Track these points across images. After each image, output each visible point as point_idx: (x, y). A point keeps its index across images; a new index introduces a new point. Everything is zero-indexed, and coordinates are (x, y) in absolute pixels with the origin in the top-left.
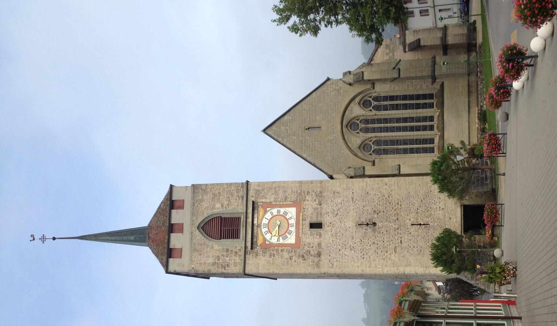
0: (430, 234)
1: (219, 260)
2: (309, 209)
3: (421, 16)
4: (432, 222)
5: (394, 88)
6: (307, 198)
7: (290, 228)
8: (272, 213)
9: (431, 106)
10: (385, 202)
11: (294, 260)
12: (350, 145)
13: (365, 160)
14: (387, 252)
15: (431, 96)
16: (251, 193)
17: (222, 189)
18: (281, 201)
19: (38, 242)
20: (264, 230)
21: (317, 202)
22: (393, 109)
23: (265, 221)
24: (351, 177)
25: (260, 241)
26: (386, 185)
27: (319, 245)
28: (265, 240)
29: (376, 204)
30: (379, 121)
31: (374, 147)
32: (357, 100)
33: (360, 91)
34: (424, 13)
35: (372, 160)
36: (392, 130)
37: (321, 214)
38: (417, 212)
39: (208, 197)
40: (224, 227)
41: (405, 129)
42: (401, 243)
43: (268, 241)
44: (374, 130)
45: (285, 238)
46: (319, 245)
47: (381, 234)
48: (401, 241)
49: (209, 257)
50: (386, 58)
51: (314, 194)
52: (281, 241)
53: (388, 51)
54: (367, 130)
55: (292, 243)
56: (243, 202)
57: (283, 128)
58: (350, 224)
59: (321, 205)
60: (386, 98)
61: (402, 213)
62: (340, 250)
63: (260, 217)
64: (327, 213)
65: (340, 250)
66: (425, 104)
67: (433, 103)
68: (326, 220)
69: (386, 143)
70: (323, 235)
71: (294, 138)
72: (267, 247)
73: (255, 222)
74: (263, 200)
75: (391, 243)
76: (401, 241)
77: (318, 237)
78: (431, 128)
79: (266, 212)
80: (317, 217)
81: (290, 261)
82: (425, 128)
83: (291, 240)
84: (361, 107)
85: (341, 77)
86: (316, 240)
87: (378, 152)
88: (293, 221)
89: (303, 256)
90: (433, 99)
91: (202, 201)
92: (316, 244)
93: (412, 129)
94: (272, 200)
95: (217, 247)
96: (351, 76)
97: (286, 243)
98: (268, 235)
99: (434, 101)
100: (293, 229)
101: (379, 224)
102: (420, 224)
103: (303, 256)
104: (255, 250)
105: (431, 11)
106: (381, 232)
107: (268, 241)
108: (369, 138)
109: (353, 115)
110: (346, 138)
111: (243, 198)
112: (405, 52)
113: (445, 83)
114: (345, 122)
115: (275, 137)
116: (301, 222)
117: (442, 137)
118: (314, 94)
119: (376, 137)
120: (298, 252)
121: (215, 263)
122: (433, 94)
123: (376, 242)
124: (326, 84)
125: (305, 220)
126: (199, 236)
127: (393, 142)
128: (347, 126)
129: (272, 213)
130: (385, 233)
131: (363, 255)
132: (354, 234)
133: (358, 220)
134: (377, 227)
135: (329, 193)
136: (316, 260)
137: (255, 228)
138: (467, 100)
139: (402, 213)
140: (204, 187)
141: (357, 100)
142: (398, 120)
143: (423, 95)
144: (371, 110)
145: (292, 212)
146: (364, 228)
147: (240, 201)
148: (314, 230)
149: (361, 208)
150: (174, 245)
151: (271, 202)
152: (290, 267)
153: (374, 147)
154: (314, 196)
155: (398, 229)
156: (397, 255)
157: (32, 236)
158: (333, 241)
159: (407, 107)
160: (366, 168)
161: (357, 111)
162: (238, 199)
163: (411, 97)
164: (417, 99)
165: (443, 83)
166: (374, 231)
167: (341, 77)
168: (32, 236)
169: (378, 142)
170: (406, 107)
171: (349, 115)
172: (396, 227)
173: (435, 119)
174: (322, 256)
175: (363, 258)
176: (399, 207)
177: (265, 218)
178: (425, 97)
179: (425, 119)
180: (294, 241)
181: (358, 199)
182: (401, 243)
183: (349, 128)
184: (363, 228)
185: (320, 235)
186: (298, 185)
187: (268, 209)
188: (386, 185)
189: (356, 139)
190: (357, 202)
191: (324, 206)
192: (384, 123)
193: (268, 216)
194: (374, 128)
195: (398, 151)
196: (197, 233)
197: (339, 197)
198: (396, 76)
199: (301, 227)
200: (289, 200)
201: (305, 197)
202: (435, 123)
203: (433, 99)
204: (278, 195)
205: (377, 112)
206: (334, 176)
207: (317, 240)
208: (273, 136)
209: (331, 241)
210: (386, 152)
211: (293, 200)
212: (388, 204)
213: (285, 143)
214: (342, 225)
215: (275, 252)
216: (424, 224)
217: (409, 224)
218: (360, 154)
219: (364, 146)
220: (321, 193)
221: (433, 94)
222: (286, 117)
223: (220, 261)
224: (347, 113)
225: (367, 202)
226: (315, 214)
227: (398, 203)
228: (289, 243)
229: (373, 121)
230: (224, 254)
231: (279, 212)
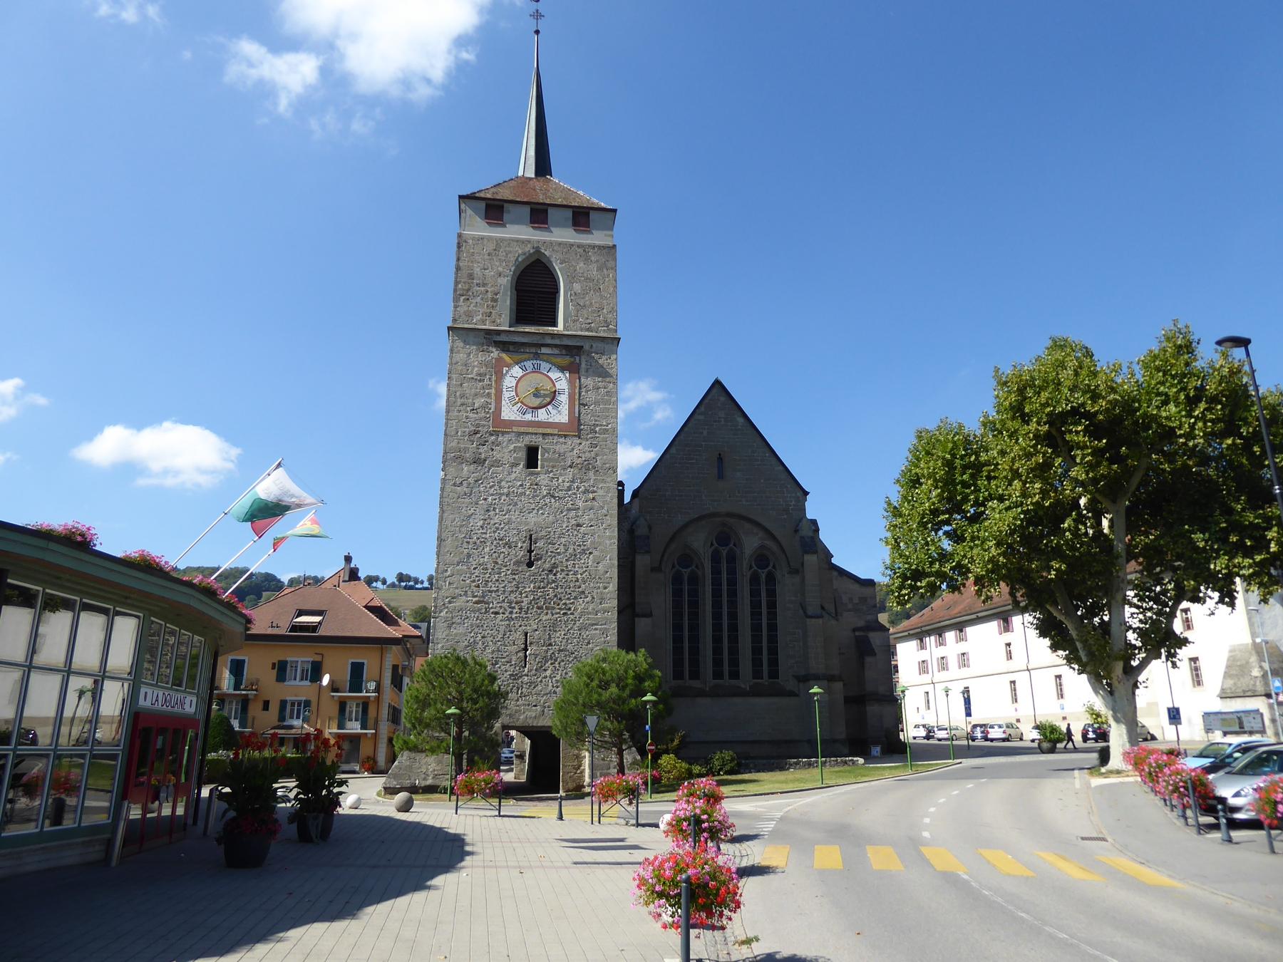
8: (559, 379)
9: (757, 674)
11: (471, 415)
15: (774, 674)
27: (497, 463)
30: (732, 583)
31: (686, 572)
32: (770, 543)
34: (923, 667)
36: (717, 605)
39: (594, 272)
40: (534, 291)
41: (717, 627)
44: (716, 572)
46: (497, 463)
50: (845, 599)
52: (506, 395)
53: (856, 601)
54: (716, 559)
60: (772, 593)
63: (554, 360)
69: (694, 593)
71: (705, 433)
73: (544, 350)
74: (583, 365)
78: (718, 675)
82: (717, 662)
85: (810, 515)
86: (506, 456)
87: (677, 579)
91: (587, 260)
93: (717, 640)
95: (502, 281)
96: (811, 534)
99: (765, 680)
102: (526, 649)
105: (926, 678)
112: (854, 630)
117: (701, 694)
126: (518, 253)
127: (694, 604)
129: (559, 379)
137: (533, 350)
139: (549, 616)
142: (733, 616)
144: (751, 567)
148: (522, 455)
150: (509, 212)
153: (686, 572)
161: (750, 543)
163: (773, 639)
164: (769, 649)
166: (518, 563)
167: (810, 515)
169: (694, 579)
170: (756, 628)
173: (733, 682)
178: (774, 663)
179: (734, 662)
189: (700, 542)
194: (719, 573)
195: (677, 613)
196: (529, 249)
198: (810, 611)
202: (727, 681)
210: (677, 593)
219: (687, 559)
222: (741, 420)
224: (747, 526)
229: (732, 571)
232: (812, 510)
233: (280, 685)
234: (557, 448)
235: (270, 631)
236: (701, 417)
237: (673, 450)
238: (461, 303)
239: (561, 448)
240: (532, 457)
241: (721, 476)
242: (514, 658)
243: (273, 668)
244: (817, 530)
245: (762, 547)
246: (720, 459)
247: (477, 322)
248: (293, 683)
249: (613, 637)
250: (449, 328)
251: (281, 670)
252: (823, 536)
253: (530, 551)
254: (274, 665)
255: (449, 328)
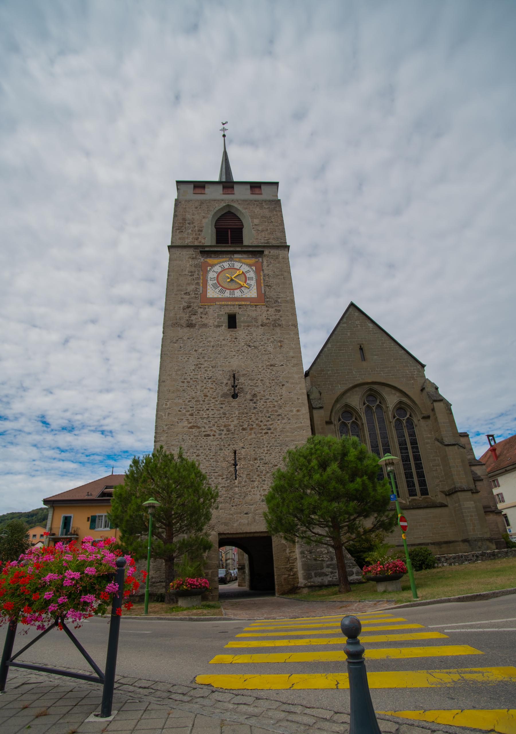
0: (220, 480)
1: (189, 224)
2: (255, 312)
3: (499, 486)
4: (240, 483)
5: (428, 443)
6: (270, 310)
7: (228, 291)
10: (270, 410)
11: (185, 296)
12: (348, 394)
13: (331, 412)
14: (192, 415)
15: (425, 492)
16: (274, 252)
17: (276, 224)
18: (264, 280)
19: (222, 126)
20: (226, 265)
21: (265, 321)
22: (400, 445)
23: (237, 265)
24: (308, 396)
25: (210, 261)
26: (298, 411)
27: (205, 326)
28: (212, 266)
29: (267, 397)
32: (405, 399)
33: (417, 402)
35: (333, 420)
37: (248, 326)
38: (256, 459)
39: (267, 213)
42: (205, 436)
43: (210, 269)
45: (215, 286)
46: (205, 326)
47: (219, 406)
48: (209, 435)
49: (193, 215)
51: (278, 317)
52: (210, 283)
55: (208, 294)
56: (262, 243)
57: (358, 322)
58: (236, 363)
59: (262, 325)
61: (253, 436)
62: (196, 351)
63: (243, 261)
64: (251, 334)
65: (196, 351)
66: (414, 485)
67: (416, 495)
68: (241, 333)
70: (218, 329)
71: (349, 334)
72: (204, 269)
75: (205, 421)
76: (209, 435)
77: (216, 323)
79: (250, 265)
80: (244, 322)
81: (183, 293)
83: (212, 293)
84: (397, 405)
88: (237, 294)
89: (189, 307)
90: (422, 495)
91: (261, 207)
92: (205, 321)
94: (266, 272)
97: (208, 287)
98: (217, 268)
100: (227, 294)
101: (235, 403)
102: (235, 465)
103: (189, 307)
104: (199, 256)
106: (223, 406)
107: (210, 269)
108: (360, 416)
109: (385, 396)
110: (357, 389)
111: (268, 243)
113: (446, 508)
114: (375, 387)
115: (347, 315)
116: (237, 303)
118: (403, 351)
119: (363, 424)
120: (194, 300)
121: (186, 221)
122: (428, 494)
123: (207, 398)
124: (417, 364)
125: (240, 308)
128: (371, 390)
129: (248, 271)
130: (222, 411)
131: (188, 382)
132: (219, 368)
133: (241, 373)
134: (231, 399)
135: (279, 335)
136: (183, 322)
138: (429, 541)
139: (253, 436)
140: (277, 209)
141: (405, 399)
143: (424, 481)
144: (394, 417)
145: (253, 293)
146: (229, 382)
147: (263, 241)
149: (260, 376)
151: (263, 270)
152: (175, 293)
154: (274, 317)
155: (228, 430)
156: (186, 429)
157: (226, 123)
158: (210, 342)
159: (406, 461)
160: (322, 411)
161: (392, 400)
162: (266, 239)
163: (419, 466)
164: (418, 473)
165: (446, 506)
166: (224, 395)
168: (226, 123)
171: (385, 393)
172: (232, 427)
174: (188, 328)
175: (183, 382)
176: (264, 431)
177: (242, 266)
178: (423, 483)
180: (211, 296)
181: (273, 373)
182: (205, 436)
183: (368, 393)
184: (229, 380)
185: (218, 326)
186: (288, 298)
187: (254, 268)
188: (298, 411)
190: (269, 371)
191: (261, 330)
192: (380, 433)
193: (245, 268)
196: (223, 204)
197: (275, 348)
199: (229, 303)
200: (267, 289)
201: (272, 308)
203: (422, 495)
204: (274, 277)
205: (393, 424)
206: (308, 378)
207: (211, 321)
208: (348, 313)
209: (210, 339)
211: (267, 293)
212: (268, 415)
213: (341, 325)
214: (234, 353)
215: (196, 276)
216: (236, 471)
217: (236, 447)
218: (338, 406)
220: (280, 325)
221: (428, 494)
222: (371, 325)
223: (187, 225)
224: (387, 389)
225: (269, 385)
226: (249, 320)
227: (270, 429)
228: (208, 291)
230: (196, 228)
231: (251, 279)
232: (429, 374)
233: (92, 531)
234: (250, 314)
235: (86, 498)
236: (345, 325)
237: (329, 345)
238: (177, 233)
239: (254, 314)
240: (232, 322)
241: (364, 359)
242: (226, 473)
243: (88, 520)
244: (437, 389)
245: (401, 402)
246: (361, 349)
247: (188, 241)
248: (100, 529)
249: (311, 433)
250: (169, 247)
251: (93, 521)
252: (441, 391)
253: (234, 386)
254: (88, 518)
255: (169, 247)
